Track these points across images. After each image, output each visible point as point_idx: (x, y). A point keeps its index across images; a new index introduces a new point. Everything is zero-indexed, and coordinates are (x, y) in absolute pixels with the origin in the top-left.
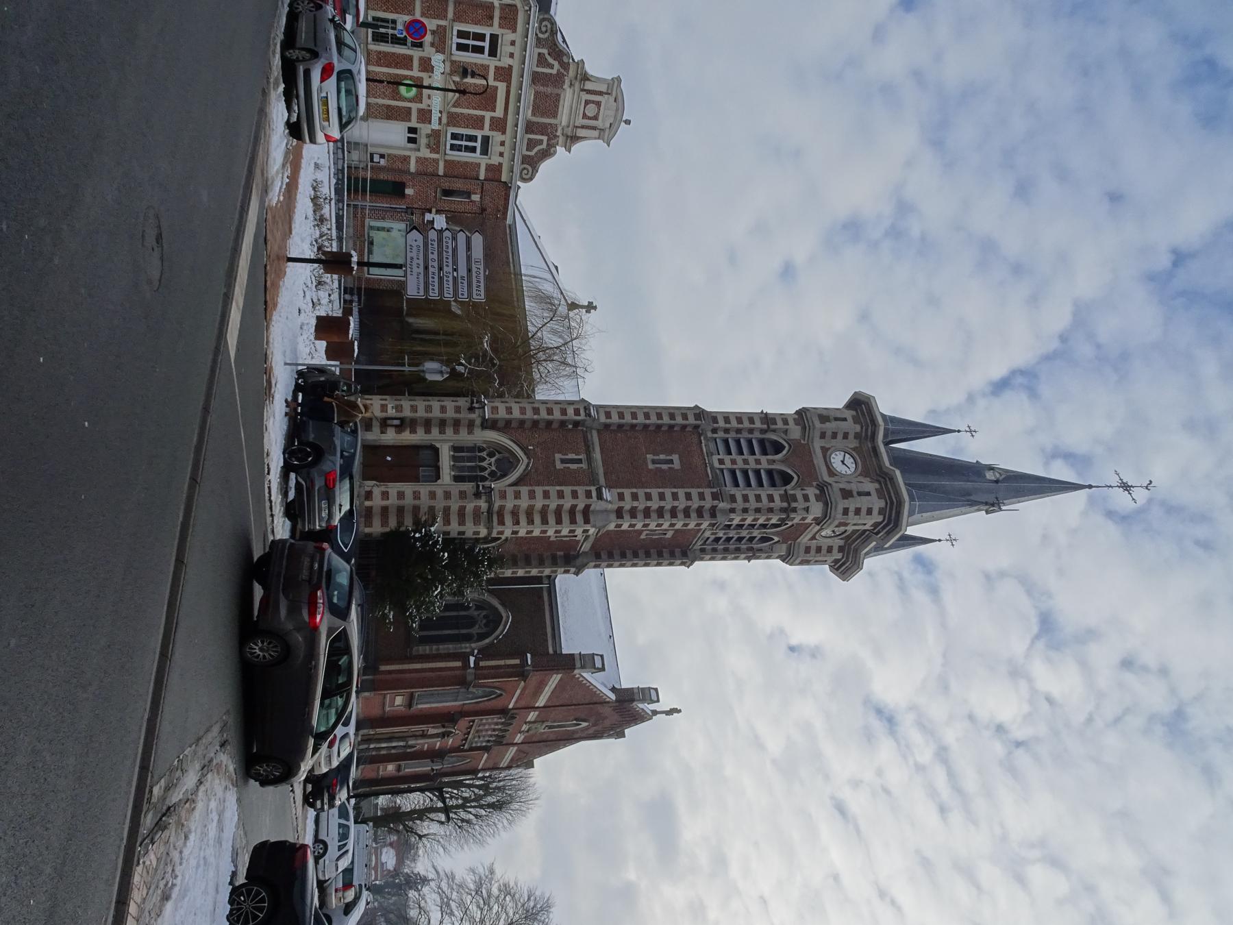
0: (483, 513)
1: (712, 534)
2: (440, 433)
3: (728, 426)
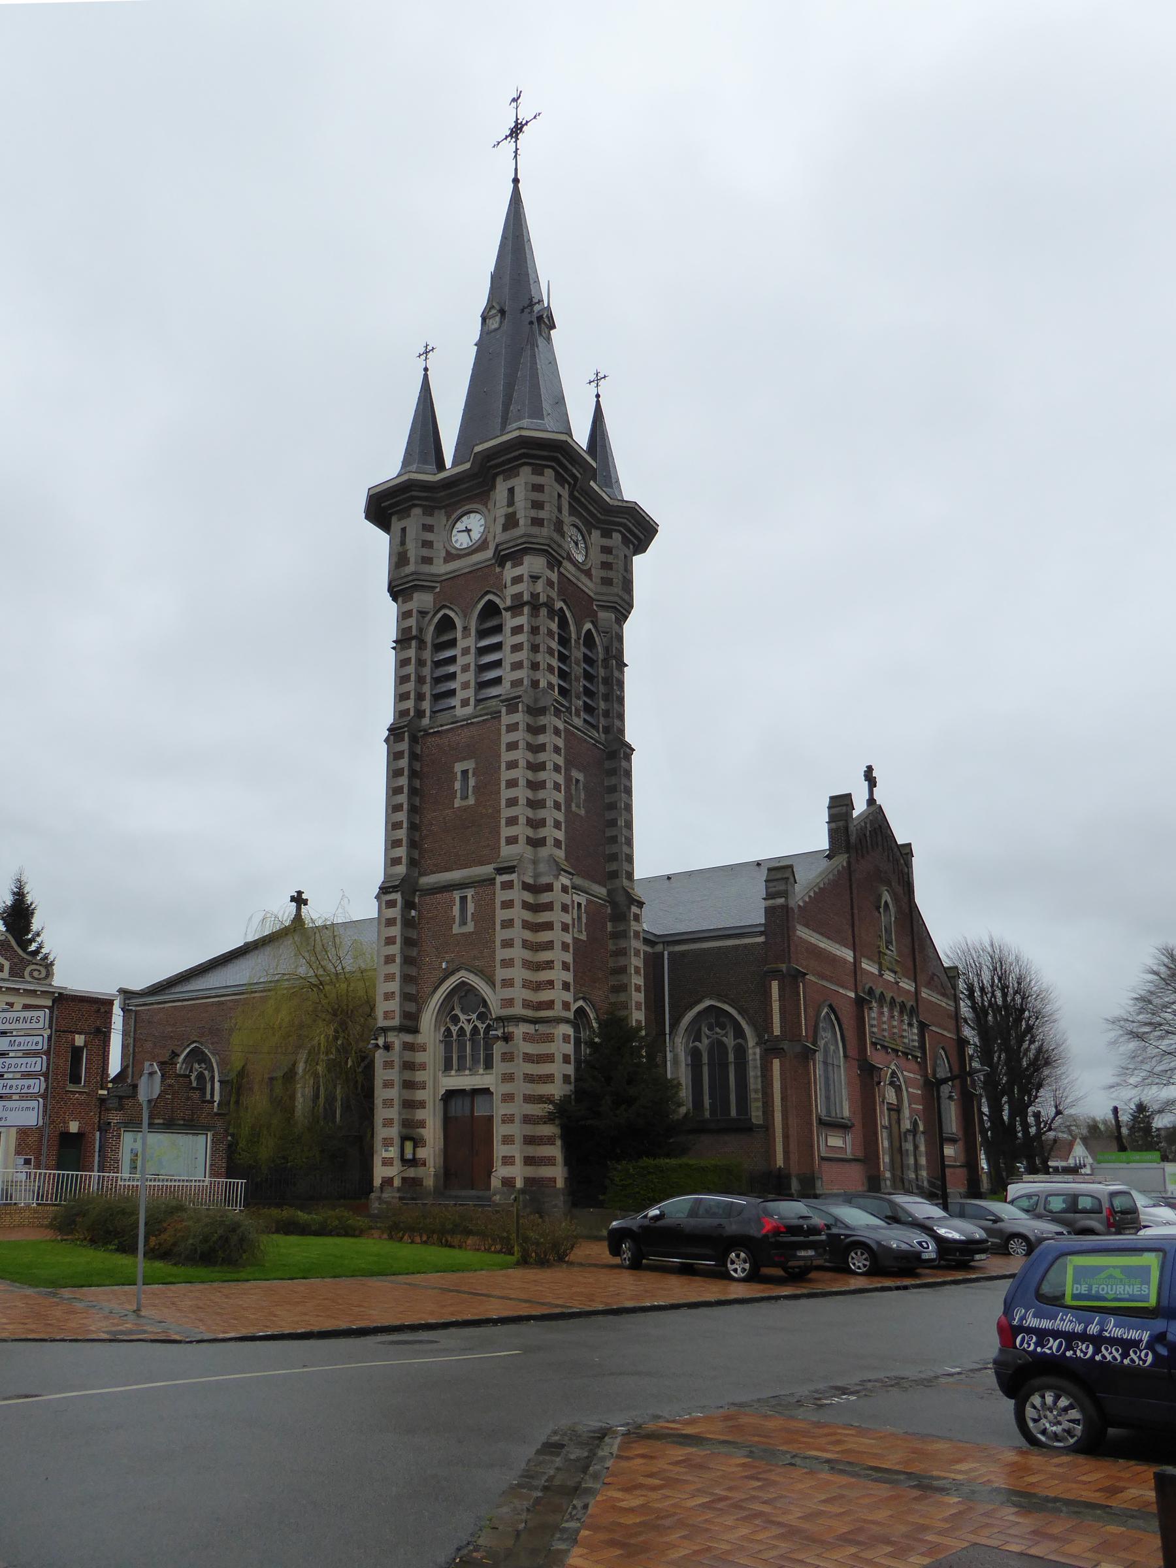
0: (536, 1030)
1: (578, 715)
2: (424, 1088)
3: (412, 696)
